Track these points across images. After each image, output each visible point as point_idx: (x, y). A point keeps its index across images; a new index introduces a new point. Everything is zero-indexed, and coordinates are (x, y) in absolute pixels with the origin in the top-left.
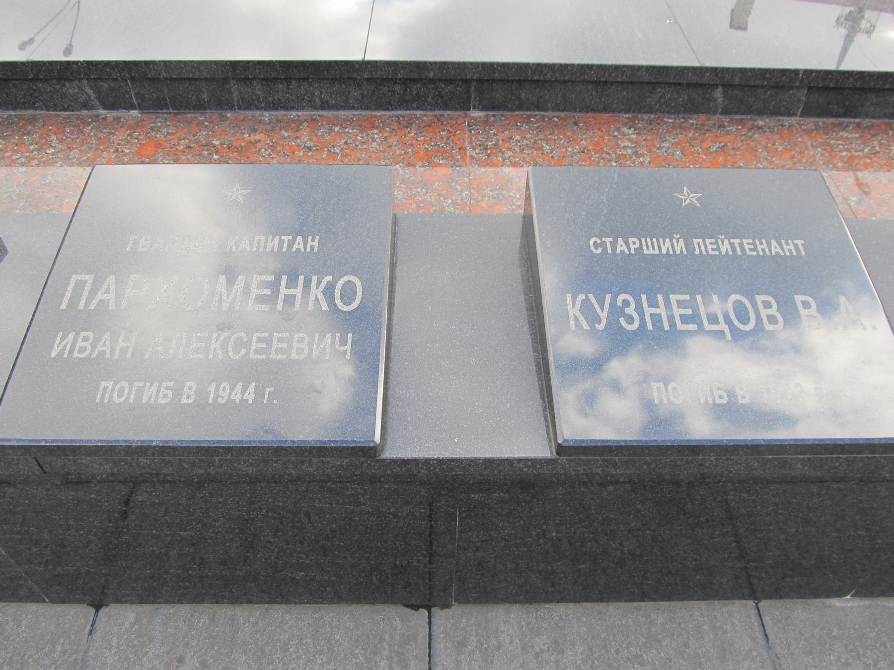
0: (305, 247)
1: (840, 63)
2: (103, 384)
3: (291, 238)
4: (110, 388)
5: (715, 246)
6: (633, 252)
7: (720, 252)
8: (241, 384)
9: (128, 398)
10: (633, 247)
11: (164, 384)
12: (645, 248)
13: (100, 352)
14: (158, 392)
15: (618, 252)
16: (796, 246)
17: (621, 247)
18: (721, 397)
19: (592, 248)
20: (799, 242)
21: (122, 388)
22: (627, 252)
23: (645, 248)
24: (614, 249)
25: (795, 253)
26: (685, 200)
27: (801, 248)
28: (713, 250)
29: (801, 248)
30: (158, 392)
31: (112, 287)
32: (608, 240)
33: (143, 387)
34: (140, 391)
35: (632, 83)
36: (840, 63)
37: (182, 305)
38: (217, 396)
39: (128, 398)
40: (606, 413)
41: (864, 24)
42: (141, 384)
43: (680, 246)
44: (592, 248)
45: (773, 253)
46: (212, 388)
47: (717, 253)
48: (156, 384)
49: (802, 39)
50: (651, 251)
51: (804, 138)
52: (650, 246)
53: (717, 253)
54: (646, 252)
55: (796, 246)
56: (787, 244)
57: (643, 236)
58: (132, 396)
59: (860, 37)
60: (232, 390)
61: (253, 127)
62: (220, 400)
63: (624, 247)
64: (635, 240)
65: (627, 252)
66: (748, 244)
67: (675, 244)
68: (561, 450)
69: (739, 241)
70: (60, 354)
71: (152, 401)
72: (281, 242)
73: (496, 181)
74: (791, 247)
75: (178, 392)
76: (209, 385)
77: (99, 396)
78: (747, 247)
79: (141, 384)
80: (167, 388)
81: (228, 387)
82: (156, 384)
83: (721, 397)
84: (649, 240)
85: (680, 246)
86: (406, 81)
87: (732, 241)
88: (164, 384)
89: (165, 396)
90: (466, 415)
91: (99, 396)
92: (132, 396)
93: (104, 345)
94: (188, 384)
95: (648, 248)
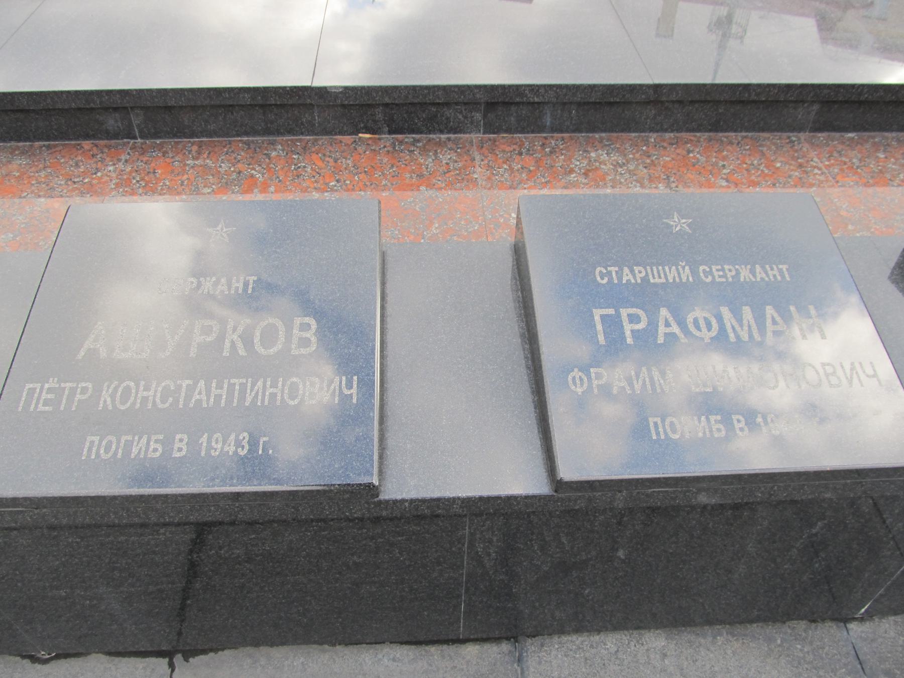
0: (229, 289)
1: (714, 78)
2: (90, 438)
3: (617, 269)
4: (97, 443)
5: (721, 273)
6: (639, 281)
7: (727, 278)
8: (206, 434)
9: (115, 454)
10: (638, 276)
11: (154, 438)
12: (651, 276)
13: (197, 401)
14: (148, 443)
15: (624, 282)
16: (780, 271)
17: (627, 276)
18: (719, 430)
19: (599, 279)
20: (784, 267)
21: (110, 442)
22: (633, 281)
23: (651, 276)
24: (620, 278)
25: (779, 278)
26: (676, 226)
27: (786, 273)
28: (720, 277)
29: (786, 273)
30: (148, 443)
31: (671, 319)
32: (613, 269)
33: (132, 442)
34: (129, 445)
35: (705, 102)
36: (714, 78)
37: (154, 350)
38: (209, 448)
39: (115, 454)
40: (594, 452)
41: (734, 29)
42: (129, 438)
43: (686, 274)
44: (599, 279)
45: (758, 279)
46: (204, 439)
47: (724, 280)
48: (144, 440)
49: (789, 52)
50: (657, 280)
51: (819, 154)
52: (662, 275)
53: (724, 280)
54: (652, 281)
55: (780, 271)
56: (772, 269)
57: (658, 265)
58: (120, 451)
59: (732, 43)
60: (224, 442)
61: (191, 159)
62: (212, 452)
63: (630, 277)
64: (641, 268)
65: (633, 281)
66: (718, 270)
67: (682, 272)
68: (559, 485)
69: (617, 269)
70: (254, 401)
71: (142, 456)
72: (231, 386)
73: (473, 211)
74: (776, 272)
75: (168, 443)
76: (202, 437)
77: (85, 452)
78: (716, 274)
79: (129, 438)
80: (156, 441)
81: (220, 439)
82: (144, 440)
83: (719, 430)
84: (655, 268)
85: (686, 274)
86: (491, 106)
87: (780, 266)
88: (154, 438)
89: (155, 450)
90: (463, 452)
91: (85, 452)
92: (120, 451)
93: (200, 393)
94: (178, 437)
95: (654, 278)
